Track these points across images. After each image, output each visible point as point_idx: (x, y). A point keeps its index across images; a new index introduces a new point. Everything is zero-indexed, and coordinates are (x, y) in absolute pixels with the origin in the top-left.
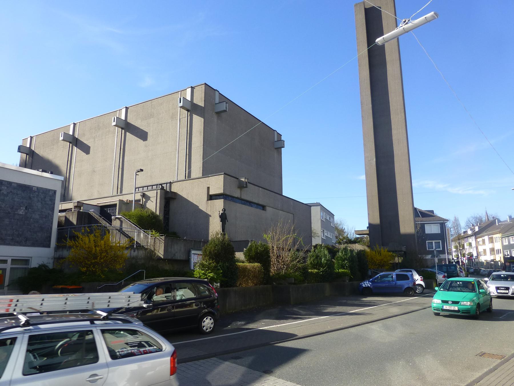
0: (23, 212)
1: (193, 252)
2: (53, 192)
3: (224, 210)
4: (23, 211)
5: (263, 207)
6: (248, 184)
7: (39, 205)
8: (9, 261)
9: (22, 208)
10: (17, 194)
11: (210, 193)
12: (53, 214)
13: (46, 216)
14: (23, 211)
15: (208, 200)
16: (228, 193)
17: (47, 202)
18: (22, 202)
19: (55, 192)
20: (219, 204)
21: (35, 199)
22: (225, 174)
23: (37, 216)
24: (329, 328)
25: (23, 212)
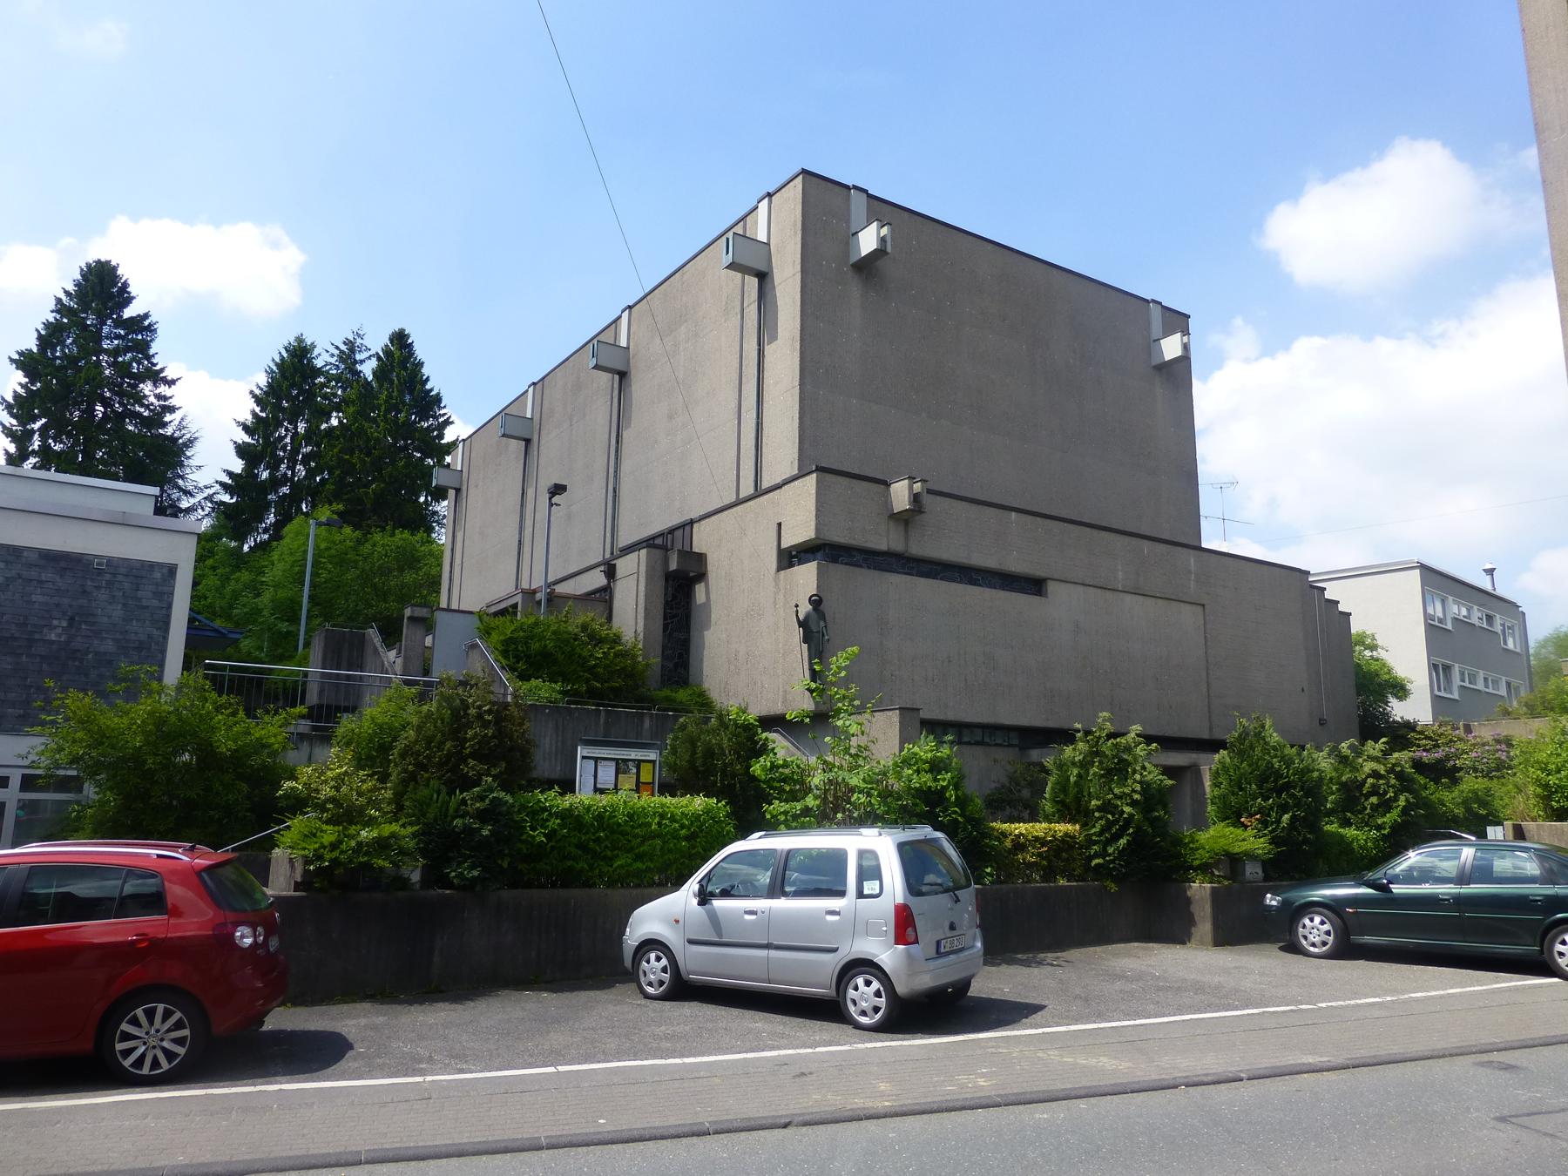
0: (59, 635)
1: (581, 751)
2: (165, 571)
3: (816, 602)
4: (59, 631)
5: (1035, 585)
6: (927, 500)
7: (117, 612)
8: (15, 782)
9: (55, 622)
10: (41, 582)
11: (784, 545)
12: (165, 638)
13: (141, 642)
14: (59, 631)
15: (780, 569)
16: (839, 537)
17: (145, 603)
18: (57, 605)
19: (171, 570)
20: (806, 577)
21: (102, 596)
22: (819, 469)
23: (109, 646)
24: (1396, 1050)
25: (59, 635)
